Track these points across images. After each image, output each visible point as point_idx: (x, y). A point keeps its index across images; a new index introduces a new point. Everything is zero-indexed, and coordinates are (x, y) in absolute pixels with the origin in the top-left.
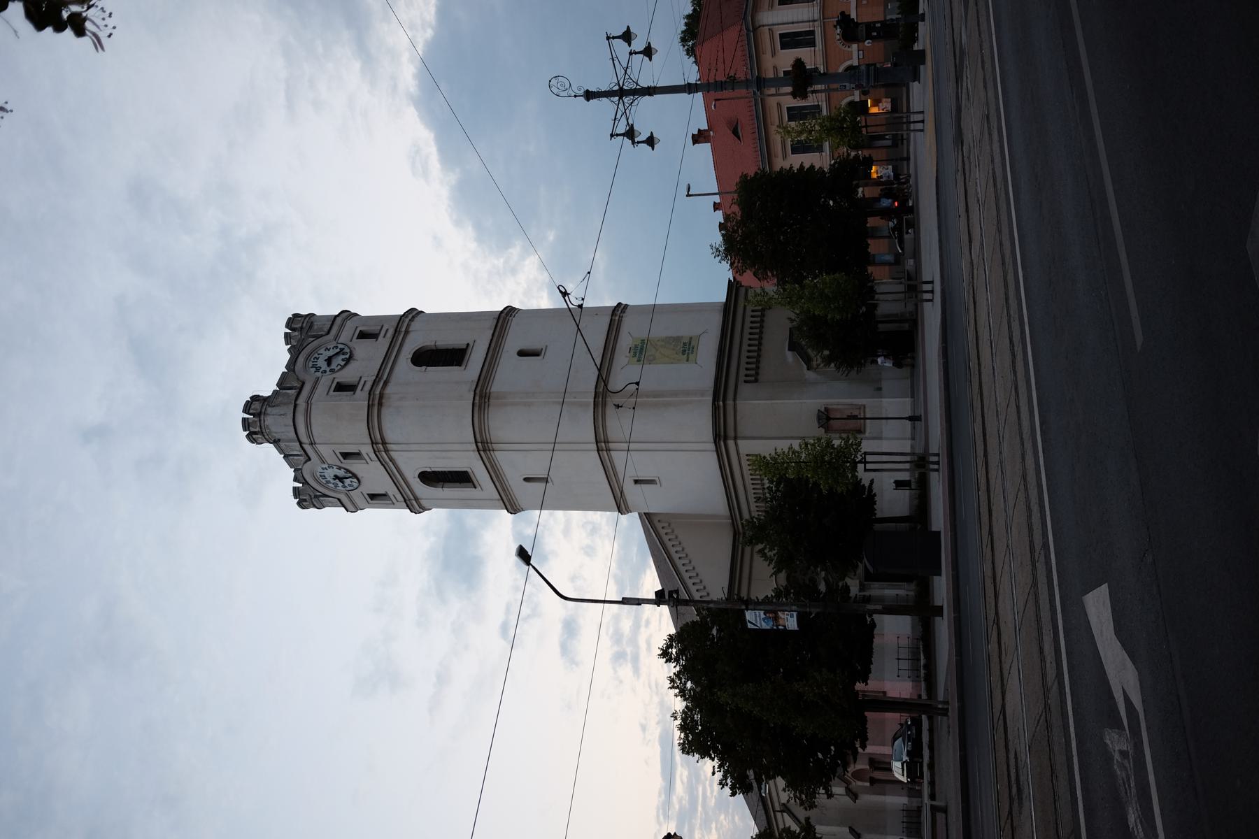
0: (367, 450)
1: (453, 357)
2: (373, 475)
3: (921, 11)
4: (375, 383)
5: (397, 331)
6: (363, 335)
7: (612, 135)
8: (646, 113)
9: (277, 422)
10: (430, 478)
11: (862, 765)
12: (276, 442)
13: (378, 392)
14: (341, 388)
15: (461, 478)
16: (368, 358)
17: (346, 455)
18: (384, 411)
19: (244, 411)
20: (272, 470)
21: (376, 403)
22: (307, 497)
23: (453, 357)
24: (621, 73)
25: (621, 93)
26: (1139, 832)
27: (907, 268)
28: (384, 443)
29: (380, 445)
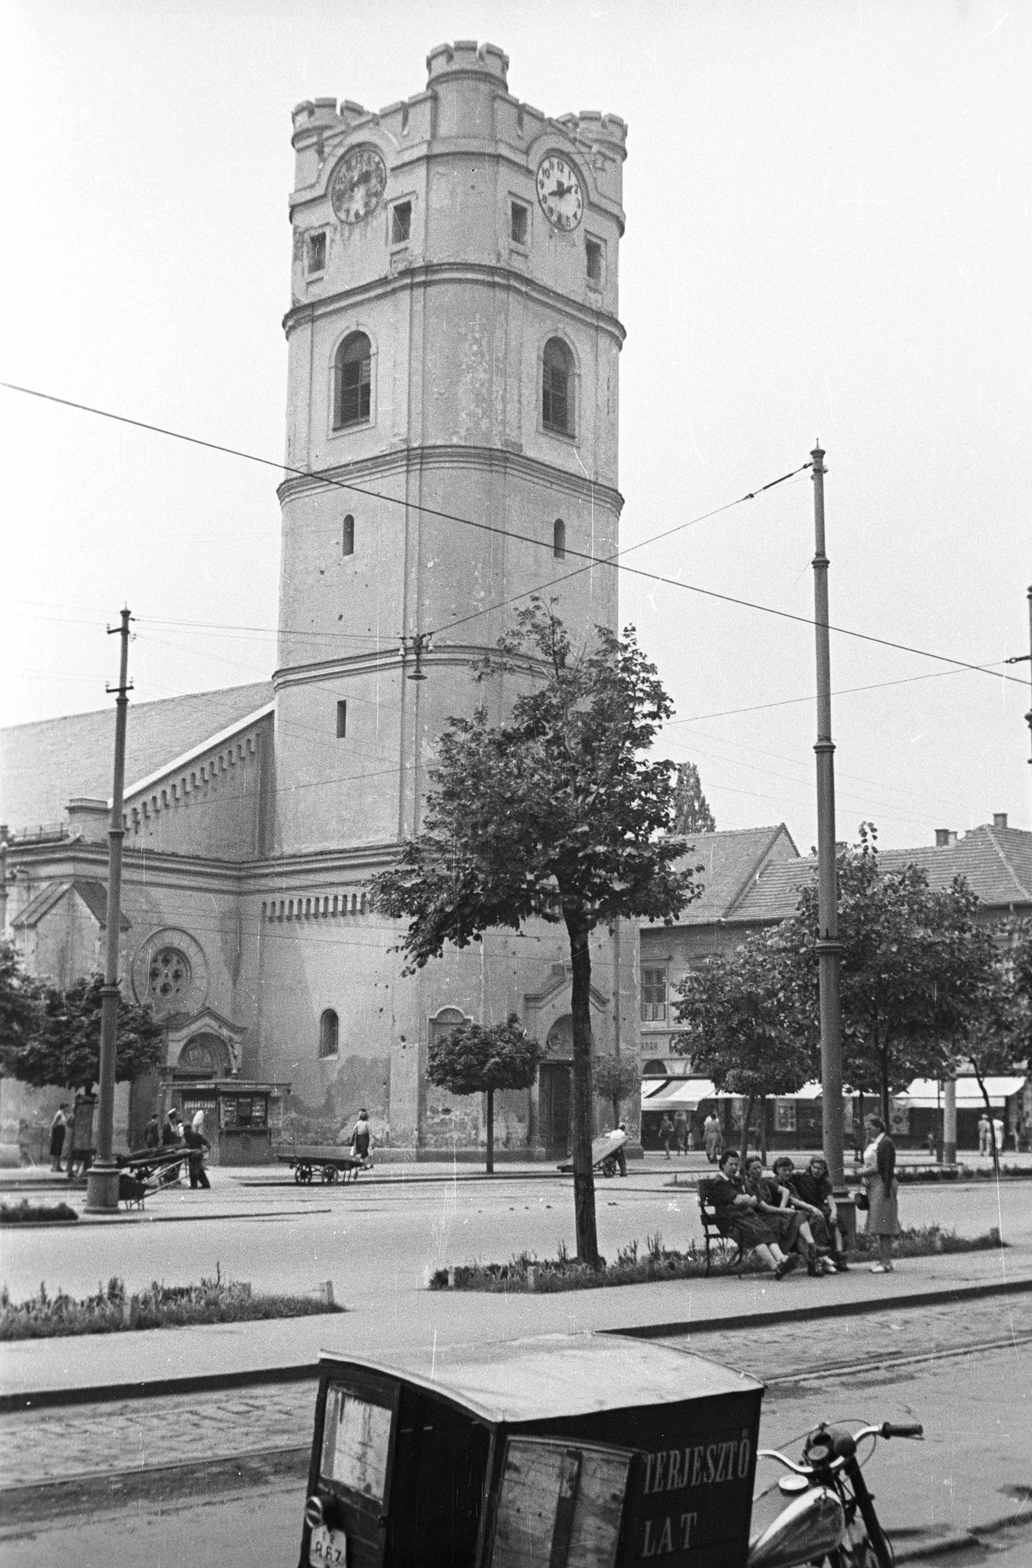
1: (556, 413)
2: (362, 256)
3: (122, 1205)
5: (599, 315)
6: (593, 250)
14: (519, 213)
15: (353, 403)
16: (555, 265)
17: (403, 212)
18: (483, 291)
20: (384, 75)
21: (504, 279)
22: (322, 127)
23: (556, 413)
26: (11, 1200)
27: (169, 1064)
28: (426, 284)
29: (418, 277)
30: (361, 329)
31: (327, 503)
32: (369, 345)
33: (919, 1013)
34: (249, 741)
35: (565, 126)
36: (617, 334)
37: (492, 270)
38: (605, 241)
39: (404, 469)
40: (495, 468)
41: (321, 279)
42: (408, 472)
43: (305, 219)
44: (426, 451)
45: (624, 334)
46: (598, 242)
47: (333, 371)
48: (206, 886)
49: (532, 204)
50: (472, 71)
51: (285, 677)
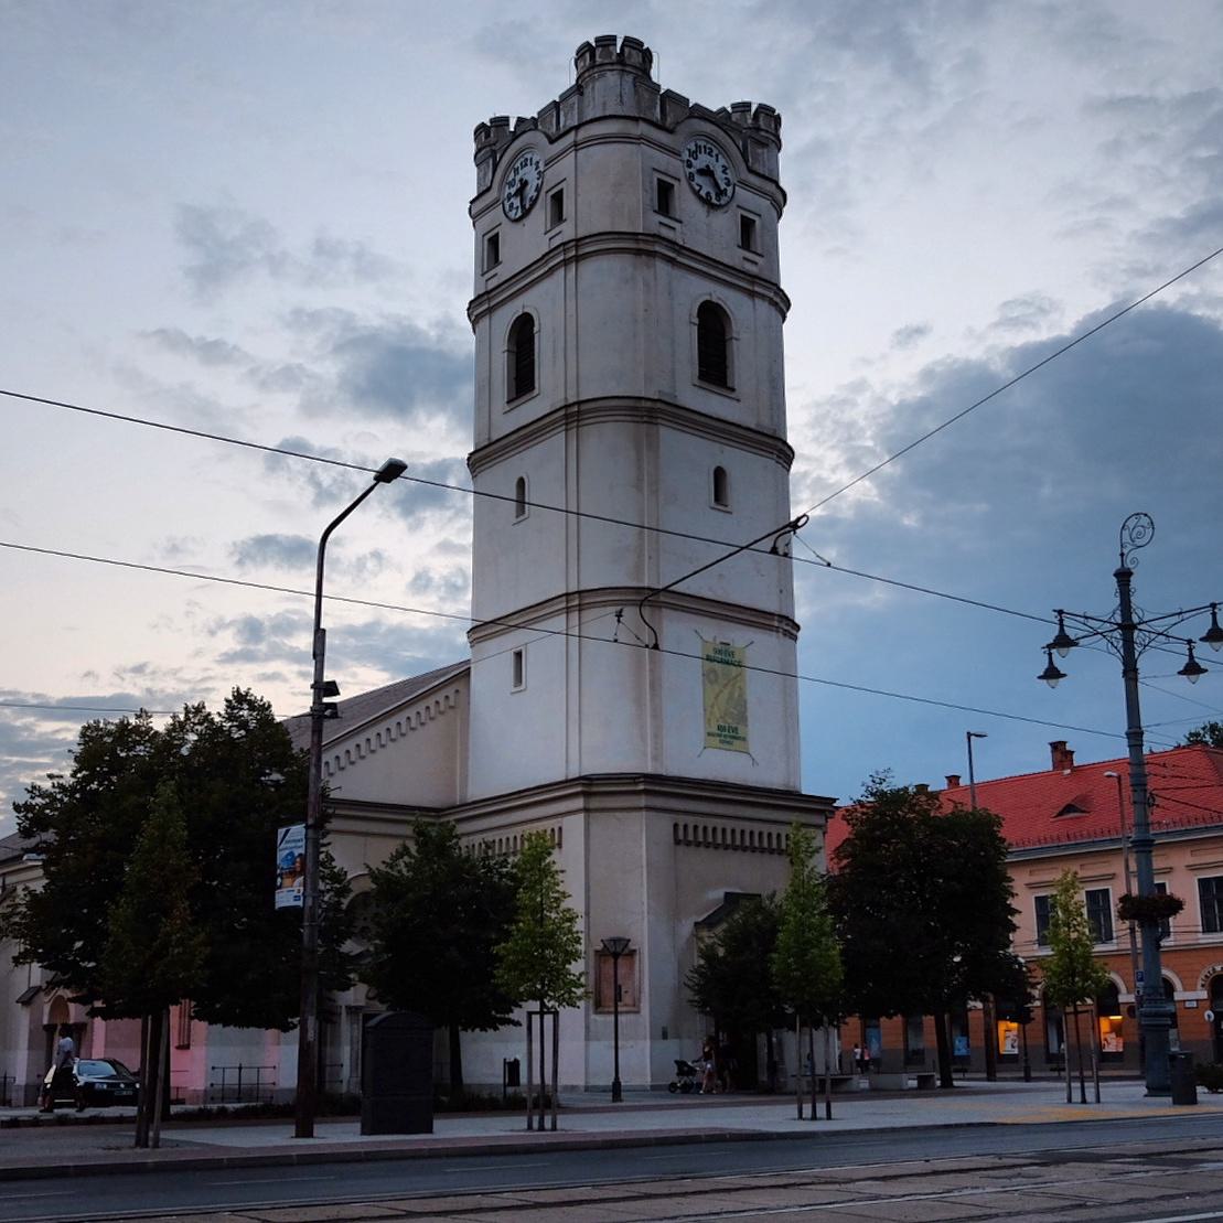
0: (567, 231)
1: (714, 365)
2: (527, 242)
4: (672, 244)
5: (754, 278)
6: (747, 226)
7: (1060, 612)
8: (1095, 666)
9: (610, 90)
10: (523, 330)
11: (76, 1013)
12: (578, 89)
13: (657, 248)
14: (665, 193)
15: (522, 381)
16: (712, 233)
19: (627, 40)
22: (494, 139)
23: (714, 365)
24: (1159, 626)
25: (1127, 627)
29: (574, 253)
30: (526, 310)
31: (502, 477)
32: (533, 325)
33: (61, 800)
34: (447, 697)
35: (721, 119)
36: (781, 304)
37: (634, 236)
38: (760, 216)
39: (564, 427)
40: (781, 461)
41: (496, 275)
42: (566, 430)
43: (487, 221)
44: (584, 407)
45: (788, 304)
46: (751, 216)
47: (506, 354)
48: (364, 830)
49: (679, 180)
50: (617, 61)
51: (481, 631)
